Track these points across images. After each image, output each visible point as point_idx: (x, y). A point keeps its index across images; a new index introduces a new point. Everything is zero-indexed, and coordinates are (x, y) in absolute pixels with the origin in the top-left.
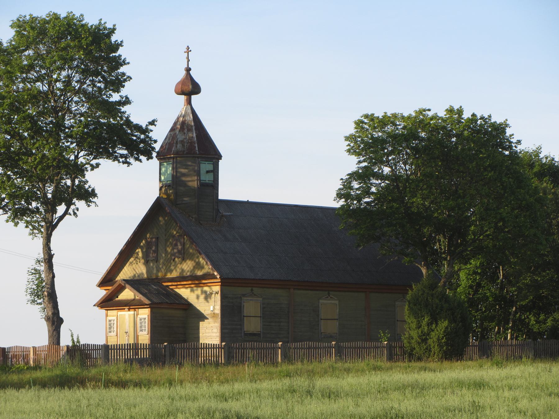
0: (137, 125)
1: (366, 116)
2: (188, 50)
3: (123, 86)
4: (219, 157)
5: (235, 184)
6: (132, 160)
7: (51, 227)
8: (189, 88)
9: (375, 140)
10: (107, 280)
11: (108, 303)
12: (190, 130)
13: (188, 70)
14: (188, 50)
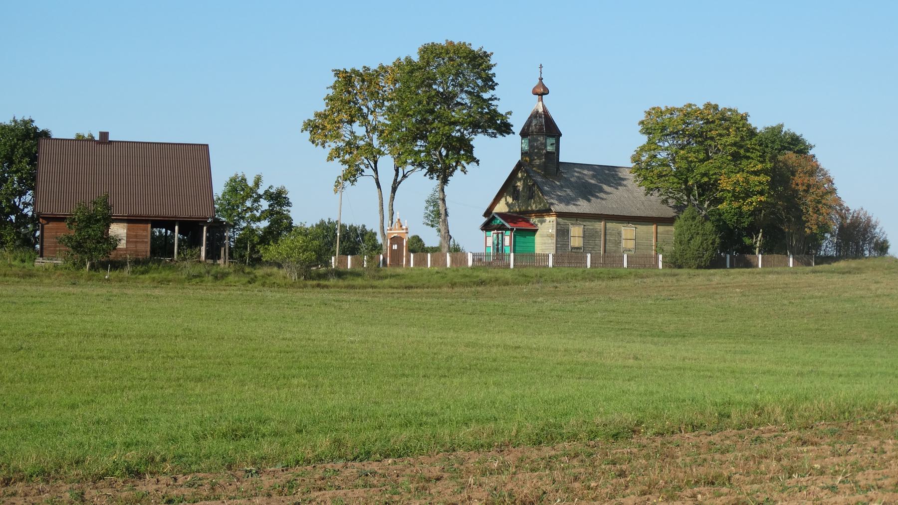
0: (775, 132)
1: (654, 109)
2: (541, 67)
3: (366, 69)
4: (560, 135)
5: (571, 151)
6: (498, 135)
7: (445, 181)
8: (541, 92)
9: (656, 126)
10: (488, 213)
11: (486, 227)
12: (540, 117)
13: (541, 79)
14: (541, 67)
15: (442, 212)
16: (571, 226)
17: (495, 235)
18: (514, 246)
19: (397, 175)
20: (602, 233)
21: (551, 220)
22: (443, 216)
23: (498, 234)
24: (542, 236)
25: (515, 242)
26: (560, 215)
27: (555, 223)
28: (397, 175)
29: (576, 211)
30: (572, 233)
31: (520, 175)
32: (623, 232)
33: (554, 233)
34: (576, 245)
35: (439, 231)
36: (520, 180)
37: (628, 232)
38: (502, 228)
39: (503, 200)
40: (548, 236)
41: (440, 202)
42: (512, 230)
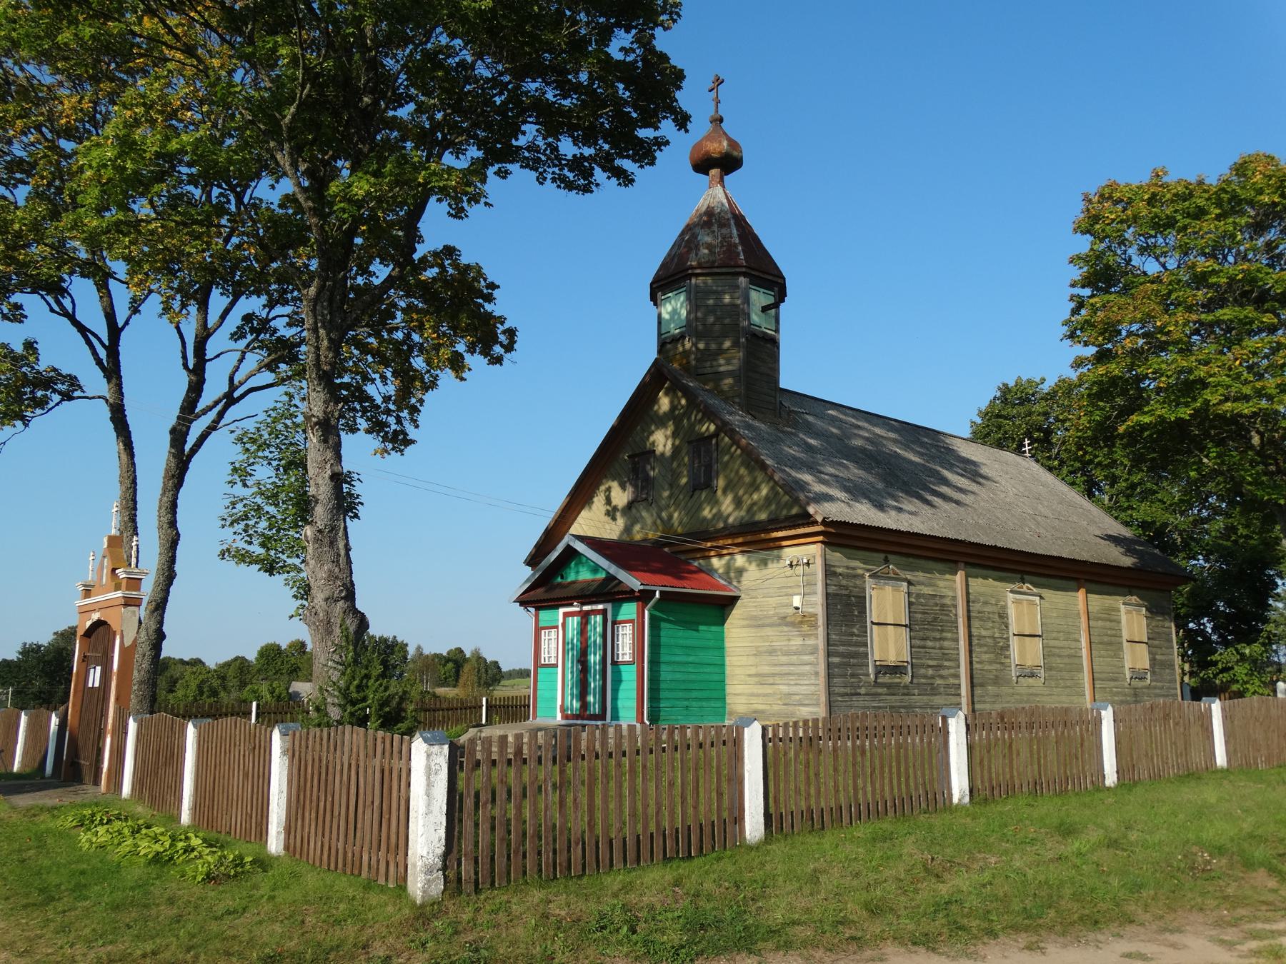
2: (719, 81)
14: (719, 81)
15: (320, 487)
16: (869, 583)
17: (574, 622)
18: (655, 663)
19: (196, 389)
20: (961, 611)
21: (805, 555)
22: (321, 513)
23: (585, 616)
24: (757, 623)
25: (655, 646)
26: (842, 536)
27: (818, 568)
28: (196, 389)
29: (904, 527)
30: (873, 614)
31: (664, 403)
32: (1012, 611)
33: (817, 604)
34: (892, 659)
35: (305, 591)
36: (661, 422)
37: (1024, 607)
38: (610, 592)
39: (599, 501)
40: (784, 621)
41: (312, 443)
42: (643, 597)
